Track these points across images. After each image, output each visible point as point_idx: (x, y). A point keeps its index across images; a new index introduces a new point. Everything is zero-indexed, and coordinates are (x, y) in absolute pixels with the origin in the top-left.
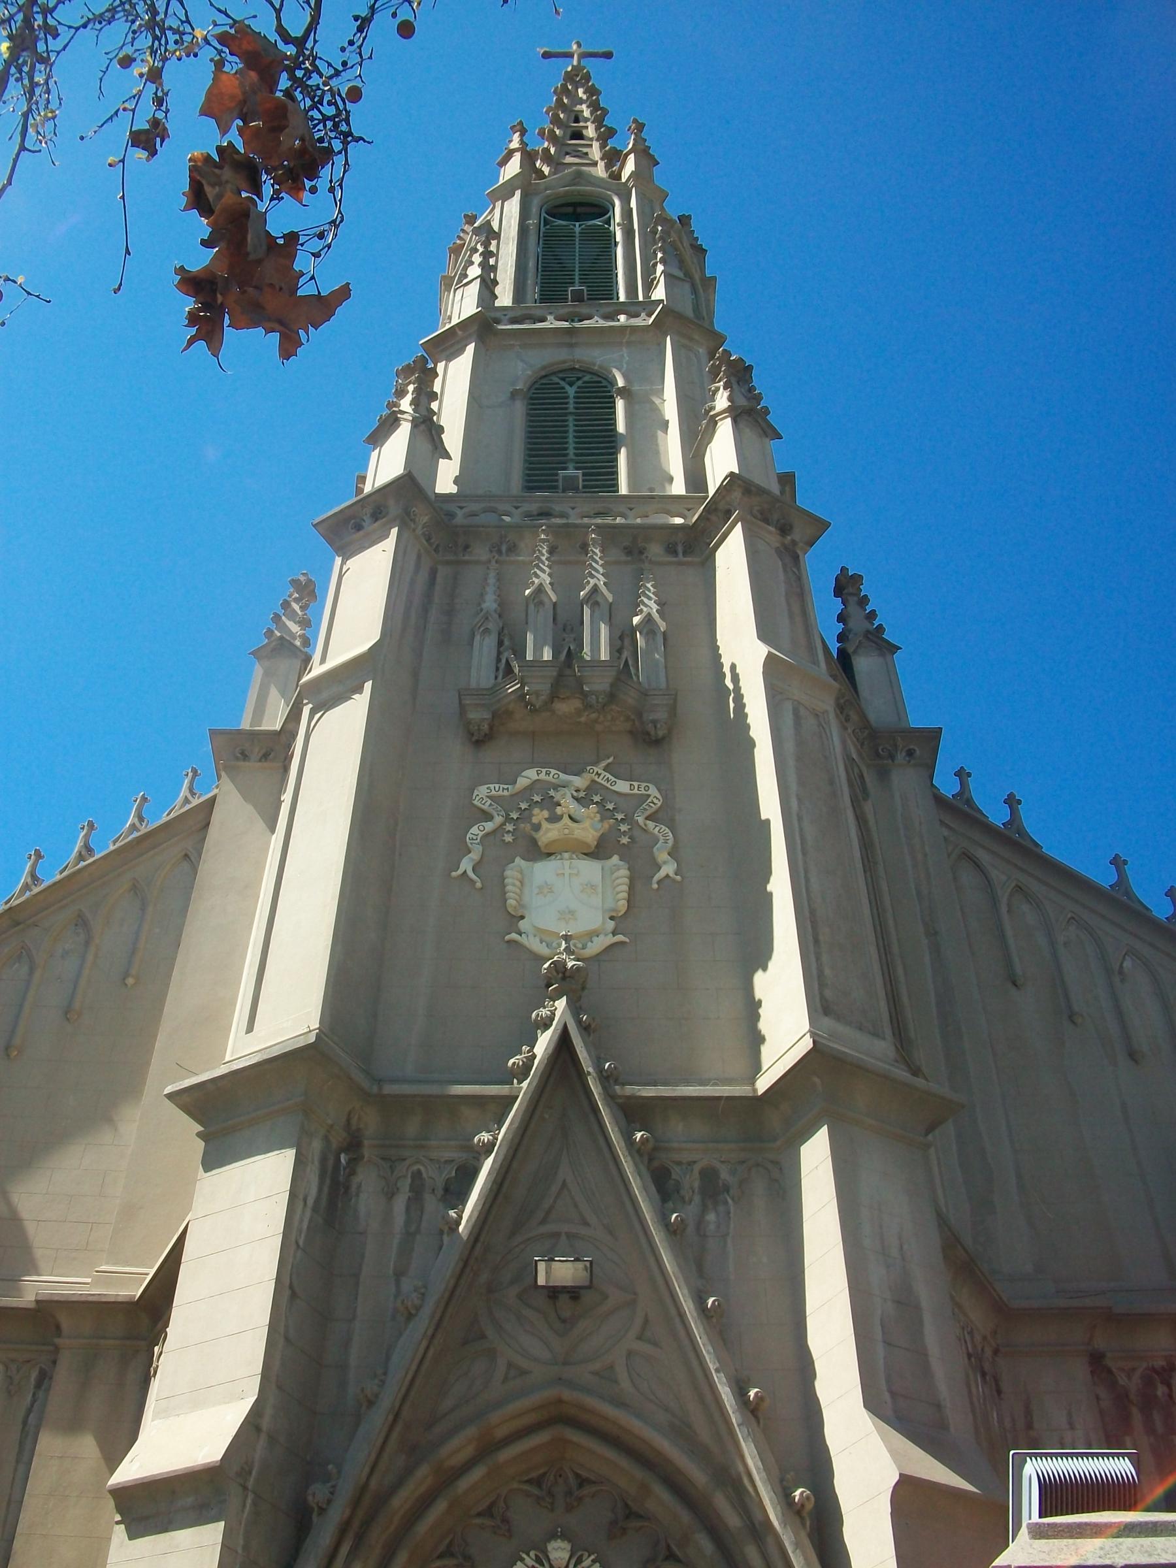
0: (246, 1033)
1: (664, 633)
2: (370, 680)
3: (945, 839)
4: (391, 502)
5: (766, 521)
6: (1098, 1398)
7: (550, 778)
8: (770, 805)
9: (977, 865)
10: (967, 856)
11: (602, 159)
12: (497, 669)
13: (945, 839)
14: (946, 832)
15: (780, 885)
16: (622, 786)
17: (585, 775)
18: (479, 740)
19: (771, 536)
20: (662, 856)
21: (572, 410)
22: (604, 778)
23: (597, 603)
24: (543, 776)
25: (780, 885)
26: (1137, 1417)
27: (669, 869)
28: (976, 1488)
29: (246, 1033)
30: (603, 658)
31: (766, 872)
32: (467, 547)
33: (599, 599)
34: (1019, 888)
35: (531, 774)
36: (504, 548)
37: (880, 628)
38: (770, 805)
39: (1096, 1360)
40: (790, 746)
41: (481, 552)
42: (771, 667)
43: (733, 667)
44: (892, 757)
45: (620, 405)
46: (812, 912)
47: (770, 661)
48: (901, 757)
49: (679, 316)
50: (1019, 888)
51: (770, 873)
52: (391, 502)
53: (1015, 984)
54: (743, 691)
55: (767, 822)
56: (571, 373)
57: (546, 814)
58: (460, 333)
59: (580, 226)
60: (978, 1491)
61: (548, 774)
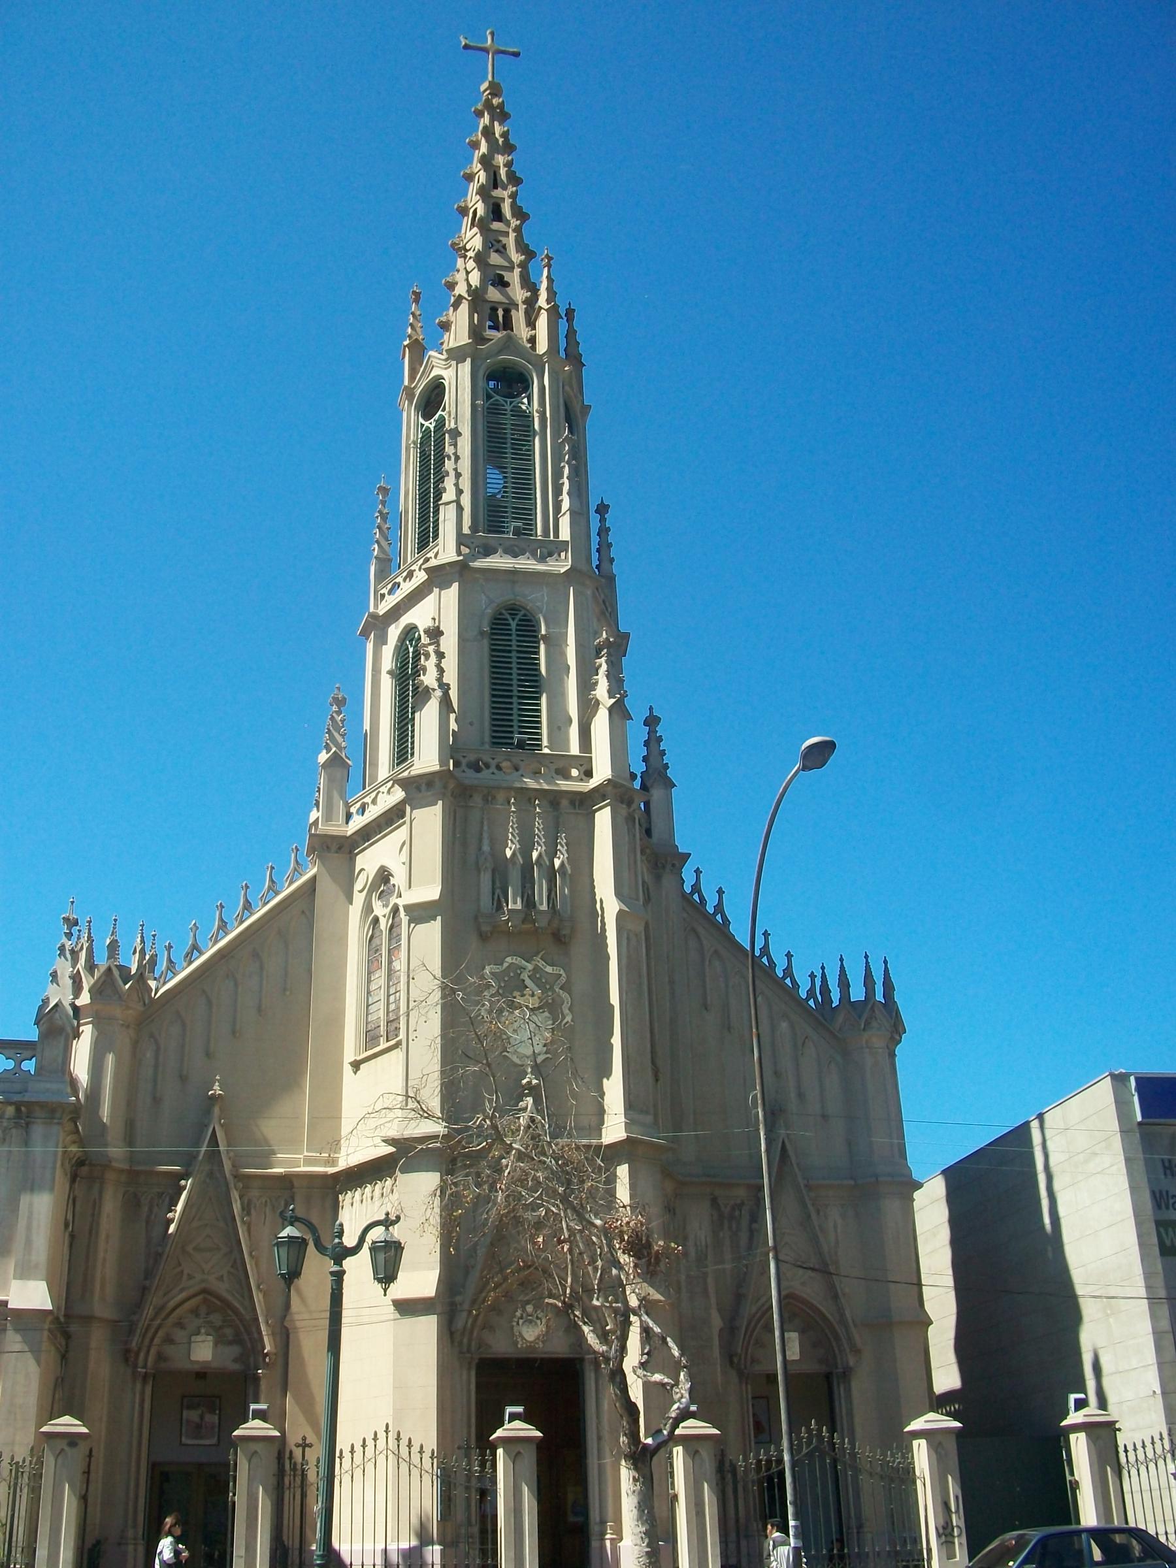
0: (355, 1073)
1: (570, 875)
2: (677, 1435)
3: (684, 919)
4: (437, 780)
5: (622, 802)
6: (712, 1215)
7: (517, 962)
8: (615, 998)
9: (698, 937)
10: (694, 930)
11: (524, 303)
12: (493, 899)
13: (684, 919)
14: (685, 915)
15: (616, 1040)
16: (549, 969)
17: (533, 962)
18: (483, 937)
19: (623, 810)
20: (566, 1011)
21: (515, 648)
22: (541, 964)
23: (541, 865)
24: (514, 961)
25: (616, 1040)
26: (726, 1222)
27: (568, 1018)
28: (628, 907)
29: (355, 1073)
30: (680, 1449)
31: (611, 1034)
32: (471, 796)
33: (542, 862)
34: (716, 952)
35: (509, 959)
36: (490, 799)
37: (666, 766)
38: (615, 998)
39: (714, 1202)
40: (624, 961)
41: (477, 799)
42: (620, 915)
43: (601, 901)
44: (664, 867)
45: (542, 647)
46: (628, 1057)
47: (620, 913)
48: (669, 867)
49: (580, 572)
50: (716, 952)
51: (613, 1034)
52: (437, 780)
53: (706, 1009)
54: (606, 927)
55: (613, 1006)
56: (513, 609)
57: (519, 993)
58: (448, 568)
59: (511, 403)
60: (627, 909)
61: (516, 959)
